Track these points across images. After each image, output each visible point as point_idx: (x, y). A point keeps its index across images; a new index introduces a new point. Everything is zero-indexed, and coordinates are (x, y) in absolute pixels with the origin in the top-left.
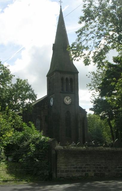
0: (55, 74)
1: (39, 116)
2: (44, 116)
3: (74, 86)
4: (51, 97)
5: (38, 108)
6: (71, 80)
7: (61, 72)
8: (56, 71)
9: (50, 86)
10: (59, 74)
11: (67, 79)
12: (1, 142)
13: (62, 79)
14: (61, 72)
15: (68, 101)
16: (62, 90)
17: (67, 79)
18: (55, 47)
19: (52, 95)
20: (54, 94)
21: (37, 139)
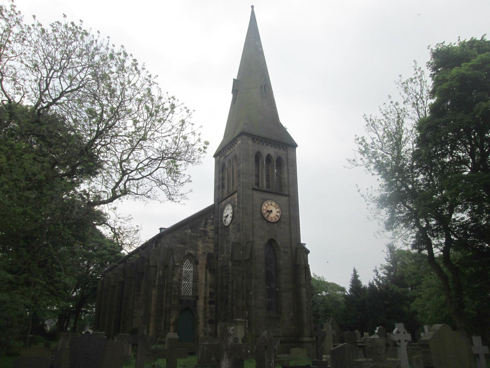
0: (240, 142)
1: (192, 252)
2: (204, 253)
3: (285, 176)
4: (225, 205)
5: (190, 231)
6: (279, 161)
7: (256, 138)
8: (242, 134)
9: (223, 178)
10: (250, 142)
11: (269, 157)
12: (443, 232)
13: (258, 156)
14: (256, 138)
15: (273, 210)
16: (257, 184)
17: (269, 157)
18: (238, 88)
19: (229, 199)
20: (236, 195)
21: (38, 62)
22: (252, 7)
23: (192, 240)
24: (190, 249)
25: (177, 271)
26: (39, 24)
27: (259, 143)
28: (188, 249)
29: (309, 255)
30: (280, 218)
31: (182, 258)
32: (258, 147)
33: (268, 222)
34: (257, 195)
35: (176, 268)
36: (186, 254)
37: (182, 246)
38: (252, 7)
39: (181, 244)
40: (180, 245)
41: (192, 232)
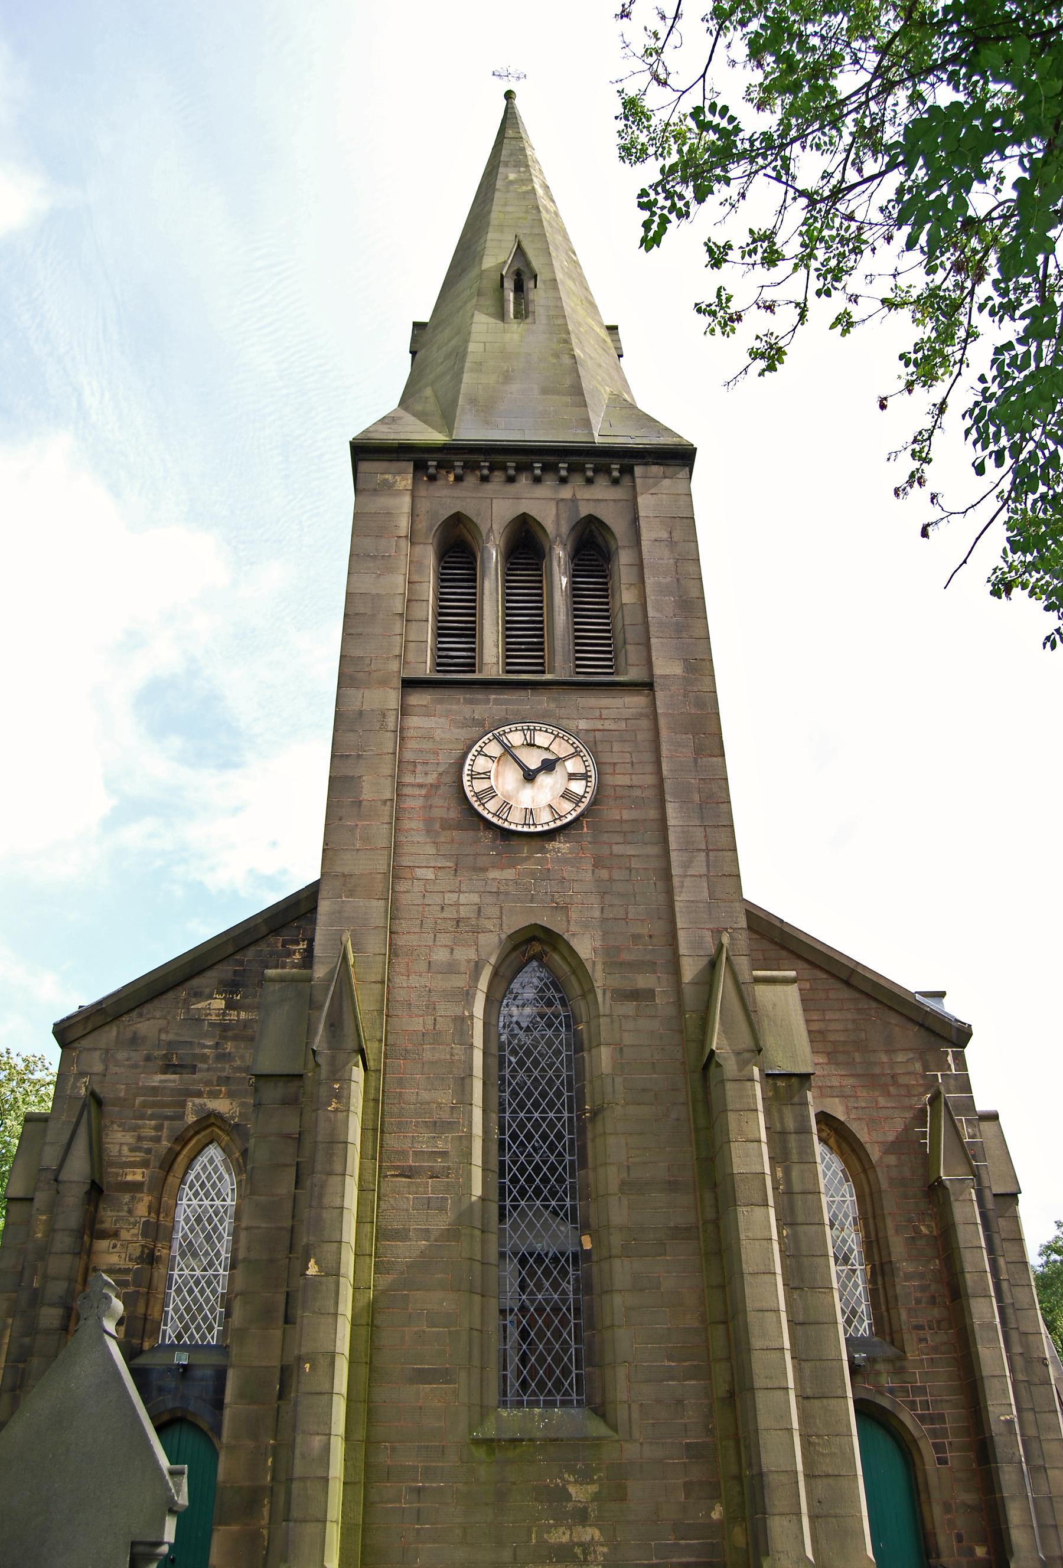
5: (219, 1003)
22: (509, 95)
23: (229, 1047)
24: (214, 1095)
25: (130, 1212)
26: (780, 352)
27: (459, 479)
28: (199, 1094)
29: (969, 1051)
30: (600, 774)
31: (165, 1144)
32: (449, 497)
33: (507, 834)
34: (435, 722)
35: (126, 1198)
36: (191, 1119)
37: (172, 1079)
38: (509, 95)
39: (168, 1068)
40: (157, 1079)
41: (230, 1005)
